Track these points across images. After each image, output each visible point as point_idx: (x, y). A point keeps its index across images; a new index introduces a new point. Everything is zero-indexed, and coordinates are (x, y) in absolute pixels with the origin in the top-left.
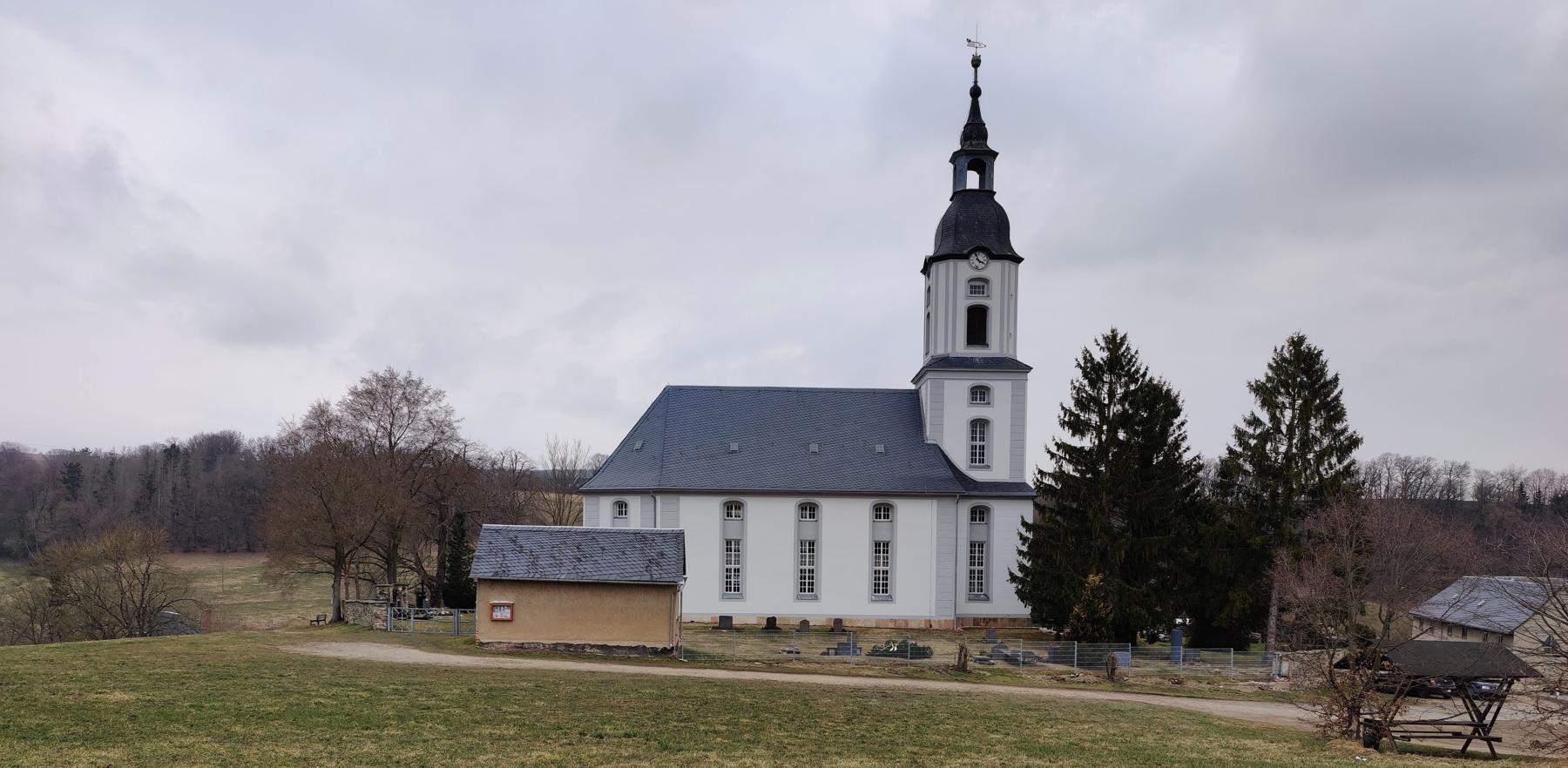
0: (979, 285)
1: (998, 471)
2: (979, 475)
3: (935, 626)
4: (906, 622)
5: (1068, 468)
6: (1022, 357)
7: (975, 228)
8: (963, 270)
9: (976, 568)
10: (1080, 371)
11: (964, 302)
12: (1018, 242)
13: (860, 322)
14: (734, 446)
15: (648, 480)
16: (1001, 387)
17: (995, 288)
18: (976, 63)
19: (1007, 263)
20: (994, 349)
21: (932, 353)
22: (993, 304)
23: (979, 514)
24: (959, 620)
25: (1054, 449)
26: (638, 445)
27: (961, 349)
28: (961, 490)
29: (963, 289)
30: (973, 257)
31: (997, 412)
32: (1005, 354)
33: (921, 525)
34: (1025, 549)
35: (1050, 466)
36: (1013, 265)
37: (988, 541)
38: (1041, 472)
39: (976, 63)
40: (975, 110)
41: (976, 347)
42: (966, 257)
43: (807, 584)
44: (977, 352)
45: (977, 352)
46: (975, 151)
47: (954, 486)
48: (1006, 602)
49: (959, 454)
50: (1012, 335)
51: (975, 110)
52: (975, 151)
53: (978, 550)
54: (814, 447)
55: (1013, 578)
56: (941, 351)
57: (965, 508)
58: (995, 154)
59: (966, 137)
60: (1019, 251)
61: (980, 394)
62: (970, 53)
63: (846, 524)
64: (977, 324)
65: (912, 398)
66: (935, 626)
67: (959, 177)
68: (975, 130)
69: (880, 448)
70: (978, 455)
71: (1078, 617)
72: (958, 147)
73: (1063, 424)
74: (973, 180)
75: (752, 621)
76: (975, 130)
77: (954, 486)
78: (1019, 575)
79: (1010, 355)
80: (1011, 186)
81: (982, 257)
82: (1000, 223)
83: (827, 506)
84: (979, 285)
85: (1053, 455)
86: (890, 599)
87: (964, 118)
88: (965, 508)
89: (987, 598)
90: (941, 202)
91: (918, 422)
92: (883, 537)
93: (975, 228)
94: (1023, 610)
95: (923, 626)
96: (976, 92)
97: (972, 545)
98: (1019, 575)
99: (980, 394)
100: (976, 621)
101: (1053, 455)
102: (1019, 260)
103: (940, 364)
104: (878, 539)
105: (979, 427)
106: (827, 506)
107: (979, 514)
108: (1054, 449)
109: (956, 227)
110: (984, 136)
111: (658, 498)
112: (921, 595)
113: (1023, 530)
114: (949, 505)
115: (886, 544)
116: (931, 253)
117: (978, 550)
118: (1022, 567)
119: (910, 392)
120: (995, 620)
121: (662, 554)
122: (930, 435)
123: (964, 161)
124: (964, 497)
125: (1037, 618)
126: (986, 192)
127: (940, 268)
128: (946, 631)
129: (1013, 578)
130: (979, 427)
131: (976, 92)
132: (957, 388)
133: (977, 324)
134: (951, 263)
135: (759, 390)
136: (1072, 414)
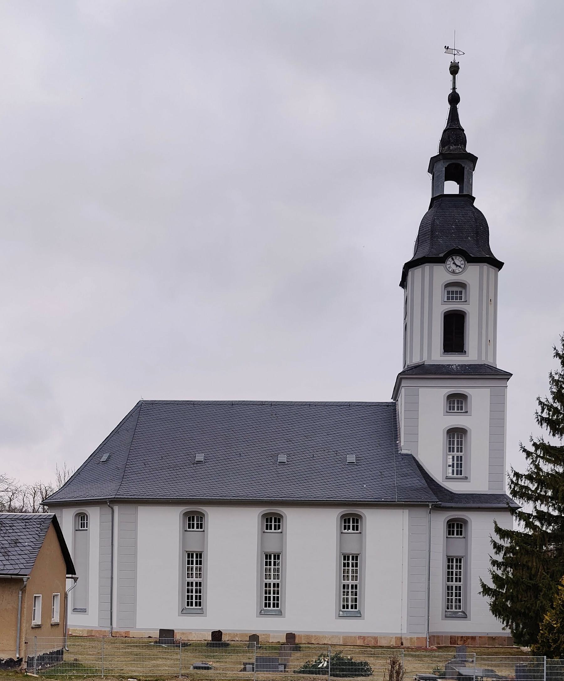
0: (456, 289)
1: (477, 483)
2: (456, 487)
3: (406, 644)
4: (376, 639)
5: (547, 468)
6: (500, 366)
7: (454, 235)
8: (441, 274)
9: (454, 584)
10: (558, 361)
11: (441, 307)
12: (497, 247)
13: (356, 356)
14: (200, 457)
15: (108, 491)
16: (479, 394)
17: (473, 292)
18: (454, 69)
19: (486, 267)
20: (472, 355)
21: (408, 363)
22: (471, 309)
23: (456, 528)
24: (434, 638)
25: (532, 449)
26: (104, 458)
27: (437, 356)
28: (435, 499)
29: (439, 294)
30: (449, 262)
31: (476, 421)
32: (483, 361)
33: (389, 534)
34: (500, 558)
35: (524, 466)
36: (492, 270)
37: (466, 556)
38: (517, 475)
39: (454, 69)
40: (454, 116)
41: (453, 357)
42: (441, 261)
43: (271, 599)
44: (454, 359)
45: (454, 359)
46: (454, 158)
47: (427, 496)
48: (483, 619)
49: (433, 458)
50: (492, 342)
51: (454, 116)
52: (454, 158)
53: (455, 565)
54: (282, 458)
55: (486, 590)
56: (416, 360)
57: (439, 522)
58: (473, 159)
59: (444, 142)
60: (499, 257)
61: (457, 402)
62: (449, 59)
63: (311, 535)
64: (454, 330)
65: (390, 410)
66: (406, 644)
67: (437, 185)
68: (454, 135)
69: (351, 458)
70: (459, 468)
71: (550, 628)
72: (436, 153)
73: (541, 421)
74: (451, 188)
75: (194, 638)
76: (454, 135)
77: (427, 496)
78: (492, 586)
79: (489, 361)
80: (488, 193)
81: (459, 260)
82: (479, 227)
83: (292, 518)
84: (456, 289)
85: (529, 454)
86: (359, 615)
87: (442, 123)
88: (439, 522)
89: (465, 616)
90: (421, 204)
91: (393, 432)
92: (351, 550)
93: (454, 235)
94: (496, 626)
95: (393, 643)
96: (454, 99)
97: (450, 560)
98: (492, 586)
99: (457, 402)
100: (453, 640)
101: (529, 454)
102: (499, 265)
103: (416, 372)
104: (347, 551)
105: (456, 435)
106: (292, 518)
107: (456, 528)
108: (532, 449)
109: (433, 231)
110: (464, 142)
111: (116, 508)
112: (392, 609)
113: (497, 538)
114: (422, 515)
115: (355, 557)
116: (410, 257)
117: (455, 565)
118: (496, 578)
119: (387, 405)
120: (473, 638)
121: (16, 542)
122: (405, 447)
123: (441, 167)
124: (437, 508)
125: (518, 638)
126: (466, 198)
127: (416, 273)
128: (418, 649)
129: (486, 590)
130: (456, 435)
131: (454, 99)
132: (431, 397)
133: (454, 330)
134: (427, 267)
135: (233, 404)
136: (550, 407)
